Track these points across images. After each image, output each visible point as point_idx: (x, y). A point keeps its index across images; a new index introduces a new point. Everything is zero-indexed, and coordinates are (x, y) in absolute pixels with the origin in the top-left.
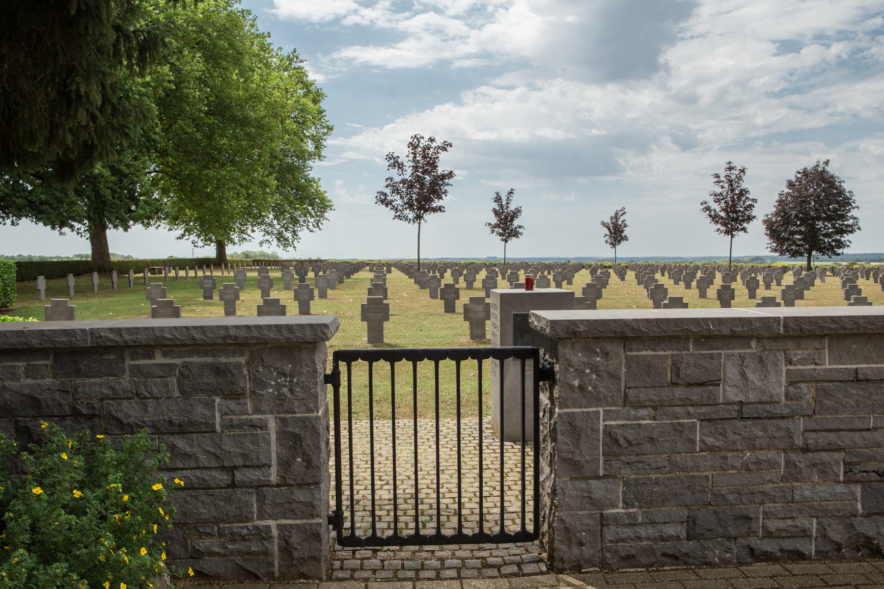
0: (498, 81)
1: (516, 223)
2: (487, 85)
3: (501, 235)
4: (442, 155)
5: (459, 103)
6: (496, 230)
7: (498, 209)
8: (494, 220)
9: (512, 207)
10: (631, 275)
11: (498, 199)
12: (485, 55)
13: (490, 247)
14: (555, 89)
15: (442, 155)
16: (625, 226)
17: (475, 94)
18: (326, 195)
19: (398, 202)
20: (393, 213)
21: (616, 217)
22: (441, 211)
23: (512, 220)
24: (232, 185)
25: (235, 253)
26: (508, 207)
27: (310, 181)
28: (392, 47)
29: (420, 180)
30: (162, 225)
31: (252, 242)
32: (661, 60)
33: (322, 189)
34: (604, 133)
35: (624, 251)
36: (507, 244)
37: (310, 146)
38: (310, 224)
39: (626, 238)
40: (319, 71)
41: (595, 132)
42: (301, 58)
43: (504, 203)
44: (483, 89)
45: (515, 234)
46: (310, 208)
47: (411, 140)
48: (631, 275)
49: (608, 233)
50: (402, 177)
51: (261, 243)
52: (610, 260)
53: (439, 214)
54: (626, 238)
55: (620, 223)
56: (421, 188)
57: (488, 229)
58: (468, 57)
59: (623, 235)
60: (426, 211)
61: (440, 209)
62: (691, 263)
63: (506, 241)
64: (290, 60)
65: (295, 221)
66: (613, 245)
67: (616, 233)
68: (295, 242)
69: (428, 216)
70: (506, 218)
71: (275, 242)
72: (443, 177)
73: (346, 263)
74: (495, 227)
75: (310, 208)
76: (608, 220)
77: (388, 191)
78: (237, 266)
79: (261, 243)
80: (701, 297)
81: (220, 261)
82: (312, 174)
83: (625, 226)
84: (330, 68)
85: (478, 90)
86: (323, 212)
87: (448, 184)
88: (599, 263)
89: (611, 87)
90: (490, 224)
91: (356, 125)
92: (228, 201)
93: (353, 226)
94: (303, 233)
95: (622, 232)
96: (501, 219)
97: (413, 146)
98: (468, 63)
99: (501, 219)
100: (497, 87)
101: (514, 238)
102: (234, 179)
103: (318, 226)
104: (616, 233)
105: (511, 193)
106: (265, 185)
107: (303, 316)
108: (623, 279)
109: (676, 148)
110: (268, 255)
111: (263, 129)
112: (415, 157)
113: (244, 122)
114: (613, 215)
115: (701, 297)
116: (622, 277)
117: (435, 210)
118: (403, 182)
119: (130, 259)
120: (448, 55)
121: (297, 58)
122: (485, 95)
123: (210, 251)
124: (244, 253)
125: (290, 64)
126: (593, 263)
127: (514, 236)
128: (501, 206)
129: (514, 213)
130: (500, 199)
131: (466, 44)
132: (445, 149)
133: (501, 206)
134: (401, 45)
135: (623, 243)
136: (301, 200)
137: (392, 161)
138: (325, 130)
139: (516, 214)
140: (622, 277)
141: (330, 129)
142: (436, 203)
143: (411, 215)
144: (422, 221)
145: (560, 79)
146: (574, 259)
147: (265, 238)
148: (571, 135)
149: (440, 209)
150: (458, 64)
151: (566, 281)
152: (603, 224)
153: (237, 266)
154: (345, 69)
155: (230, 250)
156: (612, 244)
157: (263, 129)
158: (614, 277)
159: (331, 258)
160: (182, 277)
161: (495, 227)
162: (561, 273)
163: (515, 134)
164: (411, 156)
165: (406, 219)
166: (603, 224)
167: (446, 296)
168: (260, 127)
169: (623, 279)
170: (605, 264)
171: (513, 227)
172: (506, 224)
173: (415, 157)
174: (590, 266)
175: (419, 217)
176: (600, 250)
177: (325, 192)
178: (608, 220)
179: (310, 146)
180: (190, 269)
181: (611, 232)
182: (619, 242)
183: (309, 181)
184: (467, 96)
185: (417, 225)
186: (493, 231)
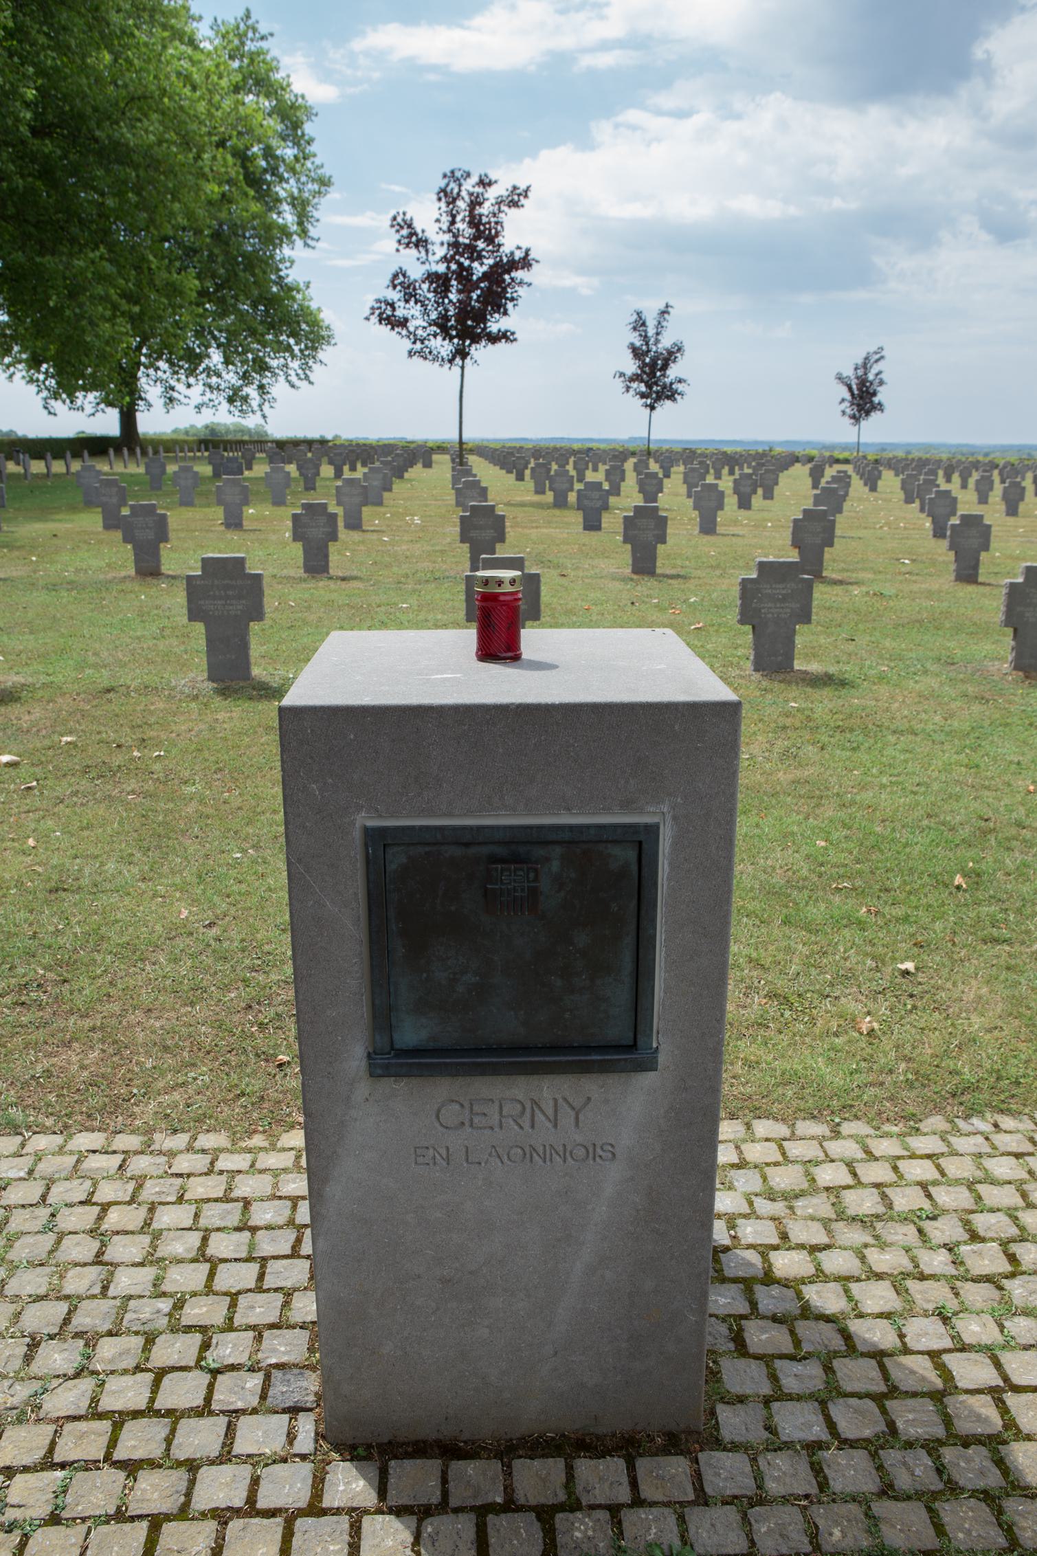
0: (666, 100)
1: (673, 372)
2: (643, 107)
3: (643, 396)
4: (510, 217)
5: (586, 143)
6: (635, 385)
7: (638, 343)
8: (631, 367)
9: (666, 342)
10: (890, 482)
11: (639, 324)
12: (636, 42)
13: (623, 420)
14: (770, 115)
15: (510, 217)
16: (881, 383)
17: (617, 126)
18: (322, 316)
19: (417, 322)
20: (407, 344)
21: (865, 365)
22: (507, 339)
23: (665, 367)
24: (100, 290)
25: (192, 426)
26: (657, 342)
27: (290, 289)
28: (462, 27)
29: (464, 275)
30: (18, 375)
31: (177, 406)
32: (979, 53)
33: (314, 305)
34: (853, 205)
35: (876, 432)
36: (655, 413)
37: (288, 217)
38: (292, 373)
39: (879, 407)
40: (325, 75)
41: (837, 203)
42: (263, 29)
43: (651, 332)
44: (633, 115)
45: (669, 393)
46: (292, 341)
47: (443, 183)
48: (890, 482)
49: (848, 396)
50: (427, 267)
51: (198, 408)
52: (845, 447)
53: (502, 345)
54: (879, 407)
55: (871, 377)
56: (470, 297)
57: (619, 384)
58: (605, 46)
59: (876, 400)
60: (476, 339)
61: (504, 336)
62: (986, 455)
63: (652, 408)
64: (242, 37)
65: (261, 367)
66: (856, 419)
67: (863, 399)
68: (266, 407)
69: (481, 352)
70: (653, 365)
71: (225, 405)
72: (513, 265)
73: (386, 449)
74: (632, 380)
75: (292, 341)
76: (849, 372)
77: (395, 295)
78: (156, 452)
79: (198, 408)
80: (980, 502)
81: (129, 439)
82: (293, 275)
83: (881, 383)
84: (349, 72)
85: (620, 119)
86: (315, 349)
87: (521, 283)
88: (827, 454)
89: (877, 113)
90: (622, 375)
91: (397, 188)
92: (91, 323)
93: (358, 381)
94: (279, 388)
95: (874, 394)
96: (645, 365)
97: (447, 197)
98: (605, 60)
99: (645, 365)
100: (659, 113)
101: (668, 403)
102: (101, 278)
103: (307, 378)
104: (863, 399)
105: (664, 313)
106: (173, 290)
107: (351, 533)
108: (873, 488)
109: (985, 237)
110: (249, 430)
111: (157, 169)
112: (453, 222)
113: (117, 154)
114: (860, 361)
115: (980, 502)
116: (872, 483)
117: (494, 339)
118: (432, 277)
119: (13, 437)
120: (566, 42)
121: (255, 30)
122: (634, 128)
123: (108, 423)
124: (207, 427)
125: (243, 44)
126: (814, 452)
127: (668, 398)
128: (645, 338)
129: (670, 353)
130: (644, 324)
131: (602, 18)
132: (514, 204)
133: (645, 338)
134: (478, 21)
135: (875, 416)
136: (272, 323)
137: (405, 232)
138: (316, 187)
139: (669, 357)
140: (872, 483)
141: (325, 182)
142: (496, 324)
143: (444, 347)
144: (468, 361)
145: (778, 94)
146: (781, 443)
147: (206, 399)
148: (792, 211)
149: (504, 336)
150: (586, 61)
151: (760, 491)
152: (840, 378)
153: (156, 452)
154: (376, 75)
155: (151, 422)
156: (853, 417)
157: (157, 169)
158: (857, 486)
159: (361, 436)
160: (37, 476)
161: (632, 380)
162: (750, 475)
163: (691, 208)
164: (446, 219)
165: (435, 359)
166: (840, 378)
167: (473, 534)
168: (154, 163)
169: (873, 488)
170: (837, 455)
171: (667, 381)
172: (653, 376)
173: (453, 222)
174: (810, 459)
175: (462, 353)
176: (831, 427)
177: (319, 310)
178: (849, 372)
179: (288, 217)
180: (55, 458)
181: (853, 395)
182: (868, 413)
183: (289, 289)
184: (603, 130)
185: (456, 370)
186: (628, 389)
